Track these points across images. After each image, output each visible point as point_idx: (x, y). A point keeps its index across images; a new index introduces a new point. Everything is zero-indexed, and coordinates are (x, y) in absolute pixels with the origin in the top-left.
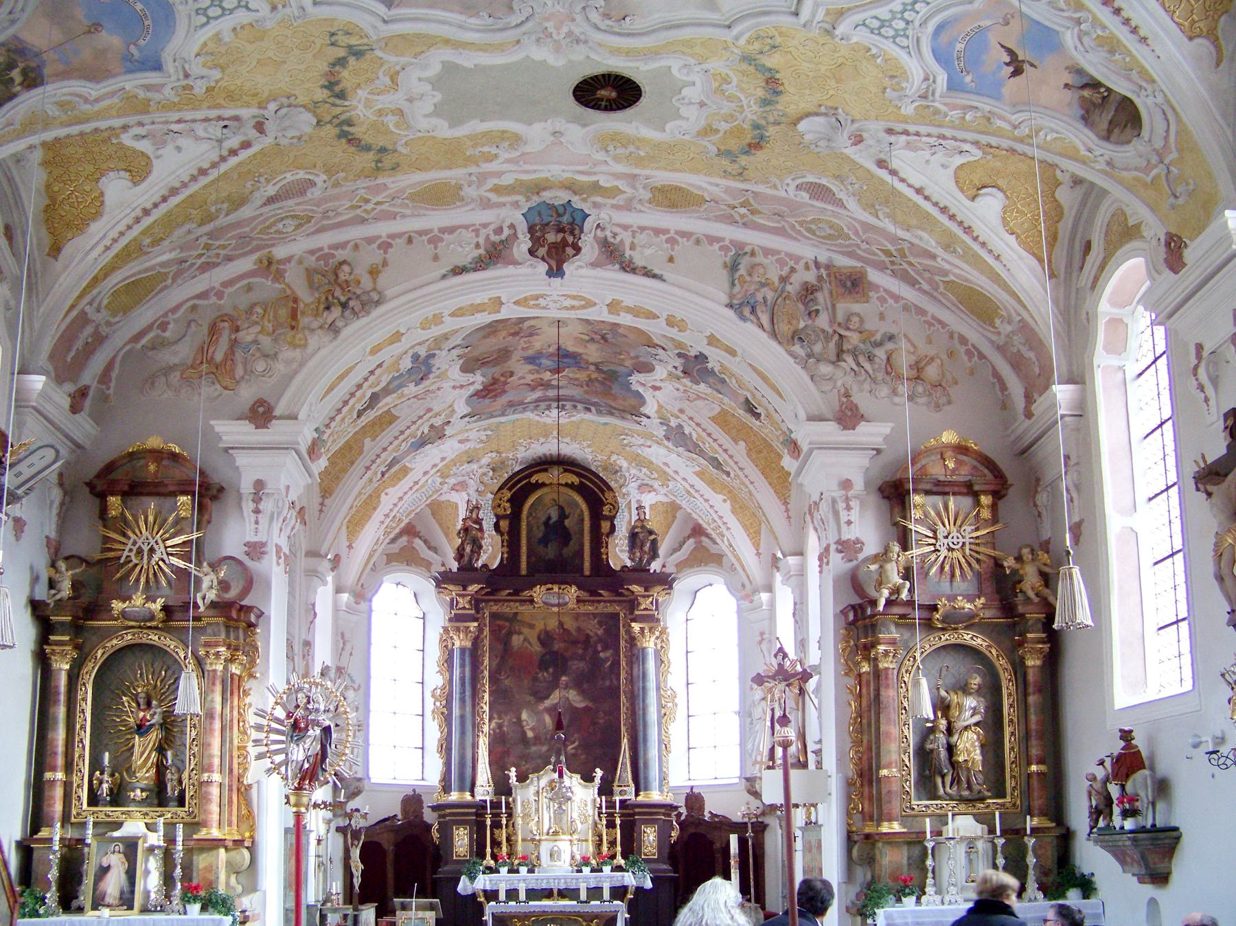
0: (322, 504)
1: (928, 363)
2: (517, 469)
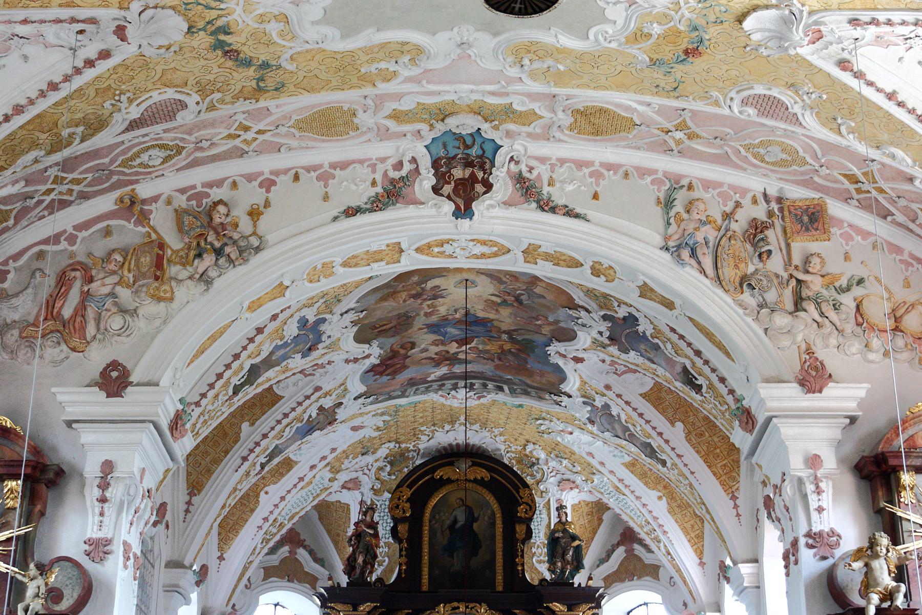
0: (189, 503)
1: (907, 311)
2: (418, 462)
